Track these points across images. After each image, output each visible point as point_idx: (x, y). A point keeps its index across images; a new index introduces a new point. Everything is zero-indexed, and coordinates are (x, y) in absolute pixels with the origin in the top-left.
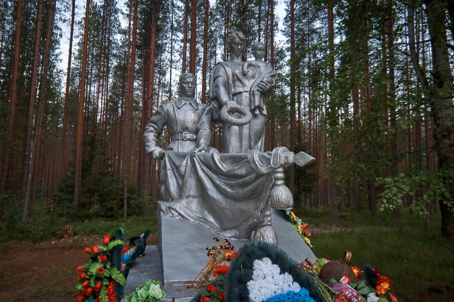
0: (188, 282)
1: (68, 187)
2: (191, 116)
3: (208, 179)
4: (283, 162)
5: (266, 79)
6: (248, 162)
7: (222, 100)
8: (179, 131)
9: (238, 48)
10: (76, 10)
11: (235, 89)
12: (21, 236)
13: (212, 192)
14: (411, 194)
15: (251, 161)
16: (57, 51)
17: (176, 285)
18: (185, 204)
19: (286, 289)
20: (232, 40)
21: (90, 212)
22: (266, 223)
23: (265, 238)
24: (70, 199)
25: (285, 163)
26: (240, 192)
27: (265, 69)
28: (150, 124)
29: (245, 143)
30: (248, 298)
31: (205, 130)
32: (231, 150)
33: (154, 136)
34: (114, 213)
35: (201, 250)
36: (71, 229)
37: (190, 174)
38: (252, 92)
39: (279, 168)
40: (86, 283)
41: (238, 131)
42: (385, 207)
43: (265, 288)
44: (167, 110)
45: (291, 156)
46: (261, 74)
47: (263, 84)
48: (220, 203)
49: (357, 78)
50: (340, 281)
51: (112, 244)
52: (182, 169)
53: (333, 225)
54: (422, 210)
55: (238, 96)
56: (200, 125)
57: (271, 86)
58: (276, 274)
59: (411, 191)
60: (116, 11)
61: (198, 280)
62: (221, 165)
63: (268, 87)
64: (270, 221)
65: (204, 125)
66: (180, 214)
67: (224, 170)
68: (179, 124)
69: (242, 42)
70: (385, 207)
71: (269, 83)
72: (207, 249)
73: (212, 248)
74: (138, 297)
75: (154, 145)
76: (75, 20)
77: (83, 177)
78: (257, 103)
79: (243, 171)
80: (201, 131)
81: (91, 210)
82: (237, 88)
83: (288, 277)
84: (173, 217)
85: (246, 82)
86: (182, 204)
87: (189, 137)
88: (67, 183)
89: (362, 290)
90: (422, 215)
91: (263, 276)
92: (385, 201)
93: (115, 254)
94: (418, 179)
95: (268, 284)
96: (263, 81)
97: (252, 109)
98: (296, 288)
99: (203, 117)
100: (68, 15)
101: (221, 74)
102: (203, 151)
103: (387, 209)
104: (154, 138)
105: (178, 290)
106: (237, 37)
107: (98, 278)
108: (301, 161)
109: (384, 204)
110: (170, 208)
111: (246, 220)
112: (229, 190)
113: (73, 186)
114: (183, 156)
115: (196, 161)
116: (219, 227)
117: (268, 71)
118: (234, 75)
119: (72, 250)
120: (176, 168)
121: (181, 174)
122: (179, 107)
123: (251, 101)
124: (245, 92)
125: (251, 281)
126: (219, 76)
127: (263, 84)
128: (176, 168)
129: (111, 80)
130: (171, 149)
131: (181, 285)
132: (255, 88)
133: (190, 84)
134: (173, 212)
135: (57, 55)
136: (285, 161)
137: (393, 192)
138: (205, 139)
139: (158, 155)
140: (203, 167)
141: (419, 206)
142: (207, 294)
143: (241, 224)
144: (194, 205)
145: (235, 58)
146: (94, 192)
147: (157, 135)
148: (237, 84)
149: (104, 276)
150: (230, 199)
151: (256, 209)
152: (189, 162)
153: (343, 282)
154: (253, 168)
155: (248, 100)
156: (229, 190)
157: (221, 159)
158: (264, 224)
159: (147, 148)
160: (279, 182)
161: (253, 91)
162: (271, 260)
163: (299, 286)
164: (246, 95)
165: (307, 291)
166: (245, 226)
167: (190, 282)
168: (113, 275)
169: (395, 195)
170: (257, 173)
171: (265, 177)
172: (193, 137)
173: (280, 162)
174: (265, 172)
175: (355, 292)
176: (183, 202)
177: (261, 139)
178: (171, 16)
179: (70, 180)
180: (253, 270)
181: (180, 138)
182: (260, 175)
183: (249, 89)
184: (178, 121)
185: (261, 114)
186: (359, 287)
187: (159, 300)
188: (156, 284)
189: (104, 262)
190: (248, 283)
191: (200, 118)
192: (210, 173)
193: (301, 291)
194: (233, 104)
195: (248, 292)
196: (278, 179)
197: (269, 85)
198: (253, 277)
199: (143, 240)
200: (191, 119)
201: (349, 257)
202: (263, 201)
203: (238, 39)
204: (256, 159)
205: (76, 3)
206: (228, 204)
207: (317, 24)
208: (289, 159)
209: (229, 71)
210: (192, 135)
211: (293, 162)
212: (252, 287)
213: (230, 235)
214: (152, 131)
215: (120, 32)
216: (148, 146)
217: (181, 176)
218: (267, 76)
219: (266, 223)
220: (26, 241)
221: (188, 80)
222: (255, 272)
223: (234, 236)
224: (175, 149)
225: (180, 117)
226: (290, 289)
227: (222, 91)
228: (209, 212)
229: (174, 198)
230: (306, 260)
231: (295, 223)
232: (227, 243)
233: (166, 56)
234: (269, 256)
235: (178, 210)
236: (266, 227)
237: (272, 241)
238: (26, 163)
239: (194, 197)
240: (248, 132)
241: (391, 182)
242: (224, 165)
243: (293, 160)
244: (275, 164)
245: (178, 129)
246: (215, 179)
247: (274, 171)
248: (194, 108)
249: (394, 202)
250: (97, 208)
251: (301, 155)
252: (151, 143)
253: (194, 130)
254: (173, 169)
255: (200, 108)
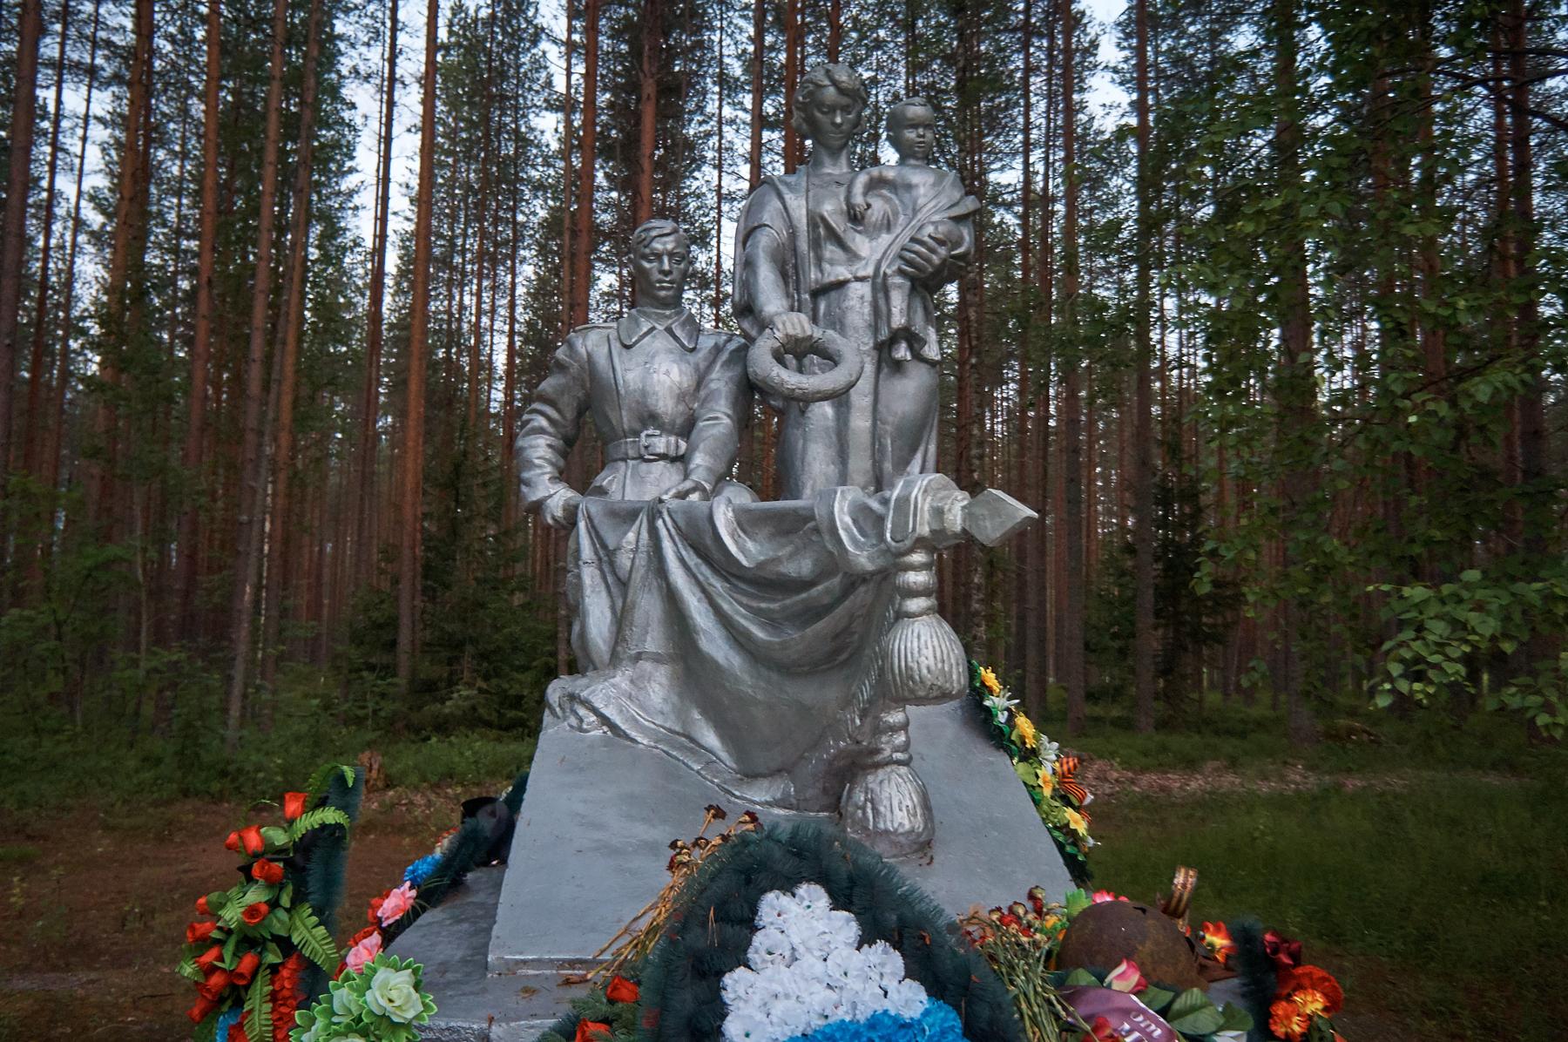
0: (572, 964)
1: (380, 626)
2: (667, 373)
3: (700, 595)
4: (925, 530)
5: (930, 229)
6: (817, 530)
7: (761, 311)
8: (626, 427)
9: (834, 124)
10: (402, 39)
11: (822, 271)
12: (215, 786)
13: (712, 640)
14: (1508, 647)
15: (824, 527)
16: (348, 183)
17: (531, 972)
18: (625, 685)
19: (869, 1003)
20: (811, 94)
21: (447, 711)
22: (887, 753)
23: (882, 809)
24: (386, 667)
25: (932, 531)
26: (797, 639)
27: (932, 193)
28: (536, 406)
29: (860, 463)
30: (719, 1032)
31: (719, 421)
32: (807, 492)
33: (550, 446)
34: (525, 716)
35: (651, 848)
36: (376, 766)
37: (645, 578)
38: (879, 280)
39: (911, 550)
40: (209, 957)
41: (831, 424)
42: (1393, 691)
43: (787, 996)
44: (589, 355)
45: (957, 507)
46: (915, 212)
47: (917, 247)
48: (737, 679)
49: (1306, 219)
50: (1107, 980)
51: (308, 822)
52: (624, 560)
53: (1295, 766)
54: (1548, 708)
55: (833, 294)
56: (702, 406)
57: (953, 257)
58: (842, 946)
59: (1507, 636)
60: (538, 33)
61: (607, 956)
62: (736, 542)
63: (936, 260)
64: (905, 748)
65: (712, 405)
66: (605, 720)
67: (745, 562)
68: (625, 403)
69: (845, 101)
70: (1393, 691)
71: (941, 243)
72: (673, 845)
73: (689, 844)
74: (334, 1014)
75: (547, 477)
76: (399, 72)
77: (429, 594)
78: (898, 320)
79: (803, 566)
80: (701, 424)
81: (448, 703)
82: (826, 266)
83: (886, 960)
84: (581, 730)
85: (861, 244)
86: (613, 685)
87: (661, 449)
88: (375, 615)
89: (1190, 1017)
90: (1546, 726)
91: (787, 954)
92: (1396, 669)
93: (317, 855)
94: (1538, 591)
95: (802, 984)
96: (919, 236)
97: (883, 343)
98: (911, 1000)
99: (714, 375)
100: (375, 57)
101: (766, 219)
102: (694, 497)
103: (1403, 704)
104: (549, 454)
105: (526, 990)
106: (827, 82)
107: (249, 941)
108: (988, 524)
109: (1391, 680)
110: (573, 697)
111: (817, 744)
112: (759, 633)
113: (392, 623)
114: (627, 516)
115: (663, 533)
116: (734, 766)
117: (944, 201)
118: (815, 220)
119: (372, 837)
120: (607, 556)
121: (619, 579)
122: (628, 343)
123: (879, 313)
124: (858, 279)
125: (741, 971)
126: (760, 226)
127: (917, 247)
128: (607, 556)
129: (527, 271)
130: (602, 491)
131: (548, 972)
132: (889, 266)
133: (666, 259)
134: (582, 711)
135: (351, 194)
136: (936, 527)
137: (1431, 638)
138: (712, 454)
139: (559, 513)
140: (684, 553)
141: (1539, 692)
142: (604, 1009)
143: (801, 757)
144: (657, 687)
145: (827, 160)
146: (460, 646)
147: (559, 443)
148: (827, 255)
149: (272, 935)
150: (769, 668)
151: (847, 702)
152: (645, 535)
153: (1116, 986)
154: (831, 553)
155: (867, 309)
156: (759, 633)
157: (739, 524)
158: (879, 758)
159: (524, 489)
160: (914, 605)
161: (885, 274)
162: (831, 894)
163: (923, 996)
164: (860, 291)
165: (953, 1015)
166: (814, 764)
167: (581, 962)
168: (297, 929)
169: (1441, 646)
170: (846, 573)
171: (872, 585)
172: (677, 447)
173: (914, 529)
174: (870, 567)
175: (1158, 1025)
176: (617, 679)
177: (922, 449)
178: (716, 38)
179: (384, 606)
180: (755, 929)
181: (631, 453)
182: (855, 580)
183: (870, 271)
184: (622, 392)
185: (918, 357)
186: (1177, 1006)
187: (406, 1026)
188: (397, 970)
189: (274, 884)
190: (728, 979)
191: (701, 380)
192: (705, 572)
193: (926, 1013)
194: (797, 324)
195: (721, 1011)
196: (912, 593)
197: (943, 251)
198: (751, 954)
199: (505, 807)
200: (668, 383)
201: (1184, 886)
202: (868, 674)
203: (832, 90)
204: (843, 518)
205: (401, 15)
206: (762, 684)
207: (1243, 38)
208: (949, 517)
209: (798, 207)
210: (673, 439)
211: (964, 530)
212: (741, 993)
213: (768, 798)
214: (541, 431)
215: (550, 107)
216: (528, 484)
217: (619, 585)
218: (936, 218)
219: (887, 753)
220: (233, 804)
221: (658, 246)
222: (758, 939)
223: (781, 800)
224: (615, 495)
225: (630, 376)
226: (887, 1004)
227: (766, 276)
228: (704, 712)
229: (598, 665)
230: (1031, 896)
231: (1030, 755)
232: (751, 826)
233: (704, 178)
234: (823, 878)
235: (599, 704)
236: (888, 769)
237: (906, 822)
238: (241, 549)
239: (657, 659)
240: (868, 424)
241: (1426, 602)
242: (750, 545)
243: (964, 520)
244: (899, 537)
245: (625, 419)
246: (721, 595)
247: (894, 563)
248: (683, 345)
249: (1431, 674)
250: (467, 698)
251: (988, 502)
252: (538, 471)
253: (679, 421)
254: (600, 559)
255: (706, 343)
